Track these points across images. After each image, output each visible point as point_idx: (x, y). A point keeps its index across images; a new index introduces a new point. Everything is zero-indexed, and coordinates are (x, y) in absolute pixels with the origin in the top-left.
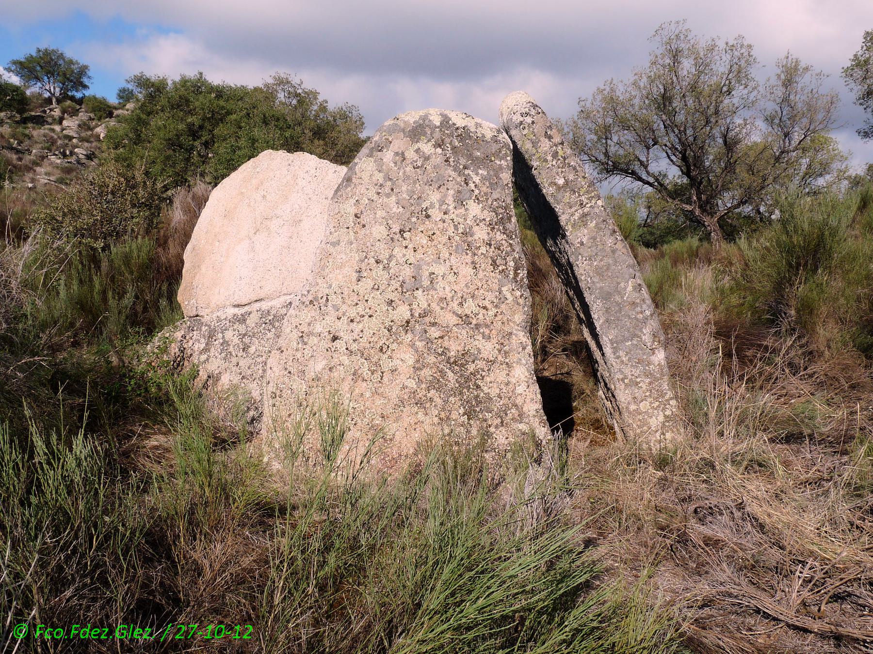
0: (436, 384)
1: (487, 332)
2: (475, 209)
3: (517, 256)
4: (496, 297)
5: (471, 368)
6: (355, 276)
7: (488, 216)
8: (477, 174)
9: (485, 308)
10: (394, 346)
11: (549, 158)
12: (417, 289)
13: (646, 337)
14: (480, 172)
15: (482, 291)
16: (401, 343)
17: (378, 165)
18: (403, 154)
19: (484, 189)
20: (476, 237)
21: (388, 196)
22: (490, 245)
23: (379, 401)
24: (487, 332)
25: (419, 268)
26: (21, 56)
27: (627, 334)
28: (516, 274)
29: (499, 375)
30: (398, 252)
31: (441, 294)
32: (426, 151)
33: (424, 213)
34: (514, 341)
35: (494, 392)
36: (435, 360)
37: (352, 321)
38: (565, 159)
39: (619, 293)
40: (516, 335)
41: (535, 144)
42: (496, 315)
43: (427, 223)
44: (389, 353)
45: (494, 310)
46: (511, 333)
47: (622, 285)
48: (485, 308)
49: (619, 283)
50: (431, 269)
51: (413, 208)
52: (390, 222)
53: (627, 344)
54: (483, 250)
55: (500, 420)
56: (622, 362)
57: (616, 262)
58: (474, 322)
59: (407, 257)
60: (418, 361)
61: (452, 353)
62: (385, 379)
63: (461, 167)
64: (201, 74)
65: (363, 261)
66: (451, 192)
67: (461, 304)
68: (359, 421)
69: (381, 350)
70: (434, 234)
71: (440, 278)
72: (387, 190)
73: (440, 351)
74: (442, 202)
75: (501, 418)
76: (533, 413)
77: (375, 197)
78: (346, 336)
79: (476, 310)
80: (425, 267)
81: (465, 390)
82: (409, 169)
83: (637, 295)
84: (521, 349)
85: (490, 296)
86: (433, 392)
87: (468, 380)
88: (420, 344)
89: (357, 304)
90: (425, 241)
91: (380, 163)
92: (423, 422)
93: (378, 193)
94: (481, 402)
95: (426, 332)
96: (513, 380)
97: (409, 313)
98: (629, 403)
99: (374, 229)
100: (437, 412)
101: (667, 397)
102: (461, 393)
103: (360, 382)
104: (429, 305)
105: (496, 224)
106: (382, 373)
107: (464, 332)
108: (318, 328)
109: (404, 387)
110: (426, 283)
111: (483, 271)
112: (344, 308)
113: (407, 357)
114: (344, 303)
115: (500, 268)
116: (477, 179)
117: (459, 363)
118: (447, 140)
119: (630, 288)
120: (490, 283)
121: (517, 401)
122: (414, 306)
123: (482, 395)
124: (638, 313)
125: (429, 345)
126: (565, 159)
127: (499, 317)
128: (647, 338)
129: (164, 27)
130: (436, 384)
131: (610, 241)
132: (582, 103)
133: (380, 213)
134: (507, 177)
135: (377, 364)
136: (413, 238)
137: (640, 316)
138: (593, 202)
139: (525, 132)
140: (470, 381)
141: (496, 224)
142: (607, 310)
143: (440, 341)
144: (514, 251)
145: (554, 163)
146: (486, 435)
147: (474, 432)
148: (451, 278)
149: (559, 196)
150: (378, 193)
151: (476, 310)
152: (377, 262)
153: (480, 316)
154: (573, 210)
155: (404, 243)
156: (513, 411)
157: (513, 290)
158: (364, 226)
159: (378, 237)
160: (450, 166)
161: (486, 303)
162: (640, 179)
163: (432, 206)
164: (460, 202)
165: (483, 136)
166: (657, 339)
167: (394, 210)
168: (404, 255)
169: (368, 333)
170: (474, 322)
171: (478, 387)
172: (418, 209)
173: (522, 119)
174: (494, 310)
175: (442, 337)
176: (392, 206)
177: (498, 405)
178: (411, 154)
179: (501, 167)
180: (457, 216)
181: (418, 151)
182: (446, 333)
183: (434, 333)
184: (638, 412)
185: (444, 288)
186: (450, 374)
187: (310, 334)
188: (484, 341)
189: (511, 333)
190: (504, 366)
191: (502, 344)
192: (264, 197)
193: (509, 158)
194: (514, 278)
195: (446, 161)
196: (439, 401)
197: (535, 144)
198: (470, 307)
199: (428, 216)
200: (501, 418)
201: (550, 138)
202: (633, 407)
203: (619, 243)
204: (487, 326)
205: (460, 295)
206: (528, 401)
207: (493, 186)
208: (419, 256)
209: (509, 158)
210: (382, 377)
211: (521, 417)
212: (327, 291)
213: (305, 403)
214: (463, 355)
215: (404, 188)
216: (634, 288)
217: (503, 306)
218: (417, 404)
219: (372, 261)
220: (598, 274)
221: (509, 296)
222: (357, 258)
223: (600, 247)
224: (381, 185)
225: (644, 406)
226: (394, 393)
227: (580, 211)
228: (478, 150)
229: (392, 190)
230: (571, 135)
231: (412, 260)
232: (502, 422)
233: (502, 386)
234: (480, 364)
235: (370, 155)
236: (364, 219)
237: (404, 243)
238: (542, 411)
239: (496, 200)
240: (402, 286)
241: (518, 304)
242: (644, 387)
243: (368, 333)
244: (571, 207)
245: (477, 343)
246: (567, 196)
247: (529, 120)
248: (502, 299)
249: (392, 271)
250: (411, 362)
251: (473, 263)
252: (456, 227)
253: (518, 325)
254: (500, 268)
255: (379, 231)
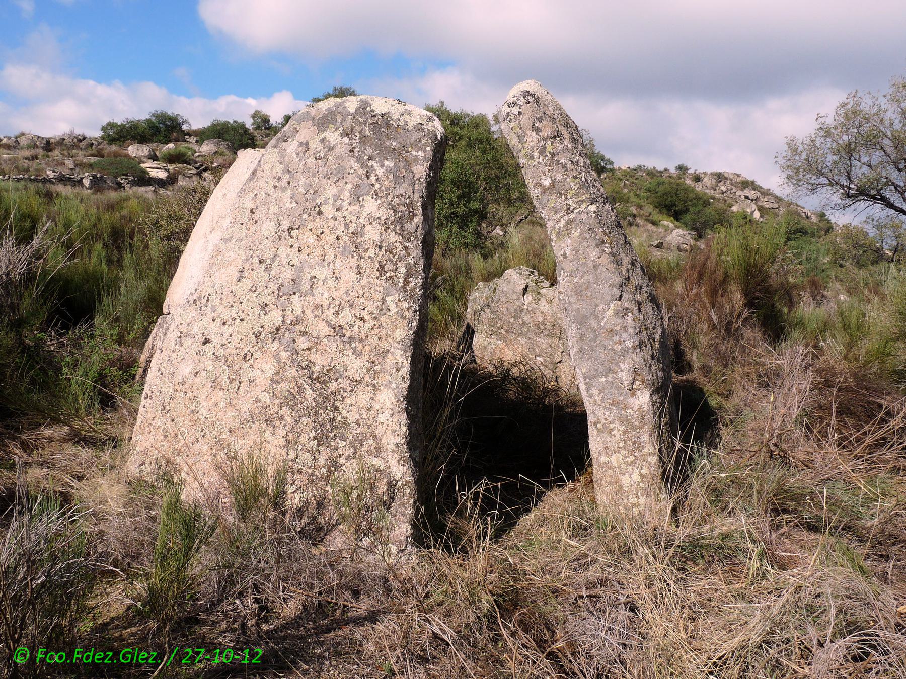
0: (291, 401)
1: (359, 346)
2: (371, 205)
3: (412, 262)
4: (377, 308)
5: (333, 386)
6: (237, 274)
7: (384, 213)
8: (382, 166)
9: (362, 319)
10: (258, 354)
11: (536, 154)
12: (294, 293)
13: (624, 374)
14: (386, 163)
15: (362, 300)
16: (266, 352)
17: (281, 157)
18: (307, 144)
19: (386, 183)
20: (366, 238)
21: (284, 189)
22: (380, 247)
23: (231, 413)
24: (359, 346)
25: (301, 270)
26: (454, 108)
27: (601, 369)
28: (407, 282)
29: (362, 398)
30: (283, 251)
31: (318, 301)
32: (332, 140)
33: (317, 209)
34: (388, 361)
35: (352, 417)
36: (296, 373)
37: (224, 324)
38: (553, 155)
39: (596, 317)
40: (393, 354)
41: (521, 138)
42: (372, 329)
43: (318, 220)
44: (251, 362)
45: (372, 323)
46: (388, 351)
47: (600, 308)
48: (362, 319)
49: (597, 305)
50: (313, 273)
51: (307, 203)
52: (281, 218)
53: (601, 380)
54: (371, 253)
55: (352, 450)
56: (595, 401)
57: (597, 279)
58: (348, 335)
59: (291, 257)
60: (277, 373)
61: (317, 368)
62: (242, 389)
63: (366, 158)
64: (442, 103)
65: (247, 260)
66: (349, 186)
67: (337, 313)
68: (208, 433)
69: (245, 357)
70: (323, 232)
71: (321, 282)
72: (284, 183)
73: (303, 364)
74: (337, 197)
75: (355, 448)
76: (392, 447)
77: (272, 191)
78: (216, 341)
79: (351, 320)
80: (307, 270)
81: (322, 411)
82: (311, 161)
83: (619, 321)
84: (394, 370)
85: (371, 306)
86: (285, 409)
87: (326, 399)
88: (284, 355)
89: (232, 306)
90: (312, 240)
91: (283, 153)
92: (268, 442)
93: (275, 187)
94: (336, 427)
95: (294, 341)
96: (377, 406)
97: (281, 319)
98: (600, 454)
99: (264, 225)
100: (285, 432)
101: (645, 450)
102: (316, 414)
103: (217, 390)
104: (303, 312)
105: (392, 224)
106: (240, 383)
107: (334, 345)
108: (195, 330)
109: (257, 401)
110: (305, 287)
111: (368, 276)
112: (221, 308)
113: (268, 368)
114: (221, 304)
115: (388, 275)
116: (380, 172)
117: (318, 380)
118: (358, 128)
119: (611, 312)
120: (372, 291)
121: (377, 432)
122: (288, 313)
123: (339, 418)
124: (615, 343)
125: (295, 356)
126: (553, 155)
127: (377, 331)
128: (625, 375)
129: (440, 61)
130: (291, 401)
131: (594, 254)
132: (822, 120)
133: (273, 209)
134: (421, 170)
135: (237, 373)
136: (301, 237)
137: (618, 347)
138: (583, 206)
139: (512, 124)
140: (329, 402)
141: (392, 224)
142: (582, 336)
143: (307, 352)
144: (409, 255)
145: (541, 160)
146: (334, 465)
147: (322, 461)
148: (331, 283)
149: (544, 200)
150: (275, 187)
151: (351, 320)
152: (260, 262)
153: (356, 329)
154: (559, 215)
155: (291, 242)
156: (370, 442)
157: (399, 300)
158: (256, 222)
159: (267, 234)
160: (353, 156)
161: (365, 314)
162: (891, 206)
163: (326, 201)
164: (357, 198)
165: (406, 124)
166: (640, 378)
167: (288, 205)
168: (288, 256)
169: (236, 338)
170: (348, 335)
171: (336, 409)
172: (313, 204)
173: (508, 110)
174: (372, 323)
175: (309, 349)
176: (285, 200)
177: (354, 432)
178: (315, 145)
179: (416, 159)
180: (351, 213)
181: (323, 141)
182: (316, 342)
183: (303, 343)
184: (608, 465)
185: (322, 295)
186: (309, 391)
187: (188, 335)
188: (354, 356)
189: (388, 351)
190: (370, 388)
191: (373, 362)
192: (225, 195)
193: (428, 149)
194: (404, 287)
195: (351, 151)
196: (289, 420)
197: (521, 138)
198: (346, 317)
199: (320, 213)
200: (355, 448)
201: (537, 130)
202: (603, 459)
203: (605, 257)
204: (361, 341)
205: (337, 303)
206: (388, 432)
207: (397, 180)
208: (304, 256)
209: (428, 149)
210: (239, 387)
211: (378, 451)
212: (209, 291)
213: (167, 408)
214: (328, 371)
215: (302, 182)
216: (616, 313)
217: (383, 319)
218: (266, 421)
219: (256, 260)
220: (576, 293)
221: (393, 309)
222: (243, 257)
223: (581, 261)
224: (280, 178)
225: (615, 460)
226: (246, 406)
227: (566, 218)
228: (394, 139)
229: (289, 183)
230: (804, 156)
231: (295, 261)
232: (355, 453)
233: (363, 412)
234: (344, 383)
235: (276, 147)
236: (258, 215)
237: (291, 242)
238: (405, 446)
239: (398, 196)
240: (279, 289)
241: (403, 317)
242: (618, 436)
243: (236, 338)
244: (556, 213)
245: (345, 358)
246: (553, 200)
247: (516, 110)
248: (383, 310)
249: (273, 272)
250: (270, 373)
251: (358, 267)
252: (347, 226)
253: (398, 342)
254: (388, 275)
255: (268, 228)
